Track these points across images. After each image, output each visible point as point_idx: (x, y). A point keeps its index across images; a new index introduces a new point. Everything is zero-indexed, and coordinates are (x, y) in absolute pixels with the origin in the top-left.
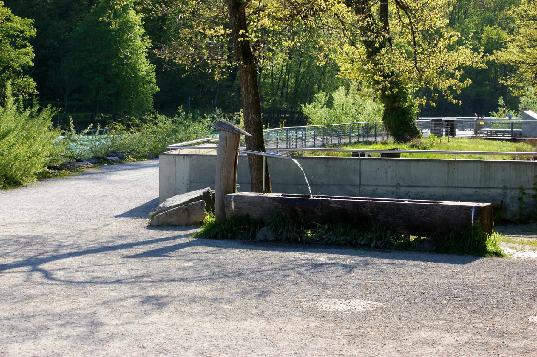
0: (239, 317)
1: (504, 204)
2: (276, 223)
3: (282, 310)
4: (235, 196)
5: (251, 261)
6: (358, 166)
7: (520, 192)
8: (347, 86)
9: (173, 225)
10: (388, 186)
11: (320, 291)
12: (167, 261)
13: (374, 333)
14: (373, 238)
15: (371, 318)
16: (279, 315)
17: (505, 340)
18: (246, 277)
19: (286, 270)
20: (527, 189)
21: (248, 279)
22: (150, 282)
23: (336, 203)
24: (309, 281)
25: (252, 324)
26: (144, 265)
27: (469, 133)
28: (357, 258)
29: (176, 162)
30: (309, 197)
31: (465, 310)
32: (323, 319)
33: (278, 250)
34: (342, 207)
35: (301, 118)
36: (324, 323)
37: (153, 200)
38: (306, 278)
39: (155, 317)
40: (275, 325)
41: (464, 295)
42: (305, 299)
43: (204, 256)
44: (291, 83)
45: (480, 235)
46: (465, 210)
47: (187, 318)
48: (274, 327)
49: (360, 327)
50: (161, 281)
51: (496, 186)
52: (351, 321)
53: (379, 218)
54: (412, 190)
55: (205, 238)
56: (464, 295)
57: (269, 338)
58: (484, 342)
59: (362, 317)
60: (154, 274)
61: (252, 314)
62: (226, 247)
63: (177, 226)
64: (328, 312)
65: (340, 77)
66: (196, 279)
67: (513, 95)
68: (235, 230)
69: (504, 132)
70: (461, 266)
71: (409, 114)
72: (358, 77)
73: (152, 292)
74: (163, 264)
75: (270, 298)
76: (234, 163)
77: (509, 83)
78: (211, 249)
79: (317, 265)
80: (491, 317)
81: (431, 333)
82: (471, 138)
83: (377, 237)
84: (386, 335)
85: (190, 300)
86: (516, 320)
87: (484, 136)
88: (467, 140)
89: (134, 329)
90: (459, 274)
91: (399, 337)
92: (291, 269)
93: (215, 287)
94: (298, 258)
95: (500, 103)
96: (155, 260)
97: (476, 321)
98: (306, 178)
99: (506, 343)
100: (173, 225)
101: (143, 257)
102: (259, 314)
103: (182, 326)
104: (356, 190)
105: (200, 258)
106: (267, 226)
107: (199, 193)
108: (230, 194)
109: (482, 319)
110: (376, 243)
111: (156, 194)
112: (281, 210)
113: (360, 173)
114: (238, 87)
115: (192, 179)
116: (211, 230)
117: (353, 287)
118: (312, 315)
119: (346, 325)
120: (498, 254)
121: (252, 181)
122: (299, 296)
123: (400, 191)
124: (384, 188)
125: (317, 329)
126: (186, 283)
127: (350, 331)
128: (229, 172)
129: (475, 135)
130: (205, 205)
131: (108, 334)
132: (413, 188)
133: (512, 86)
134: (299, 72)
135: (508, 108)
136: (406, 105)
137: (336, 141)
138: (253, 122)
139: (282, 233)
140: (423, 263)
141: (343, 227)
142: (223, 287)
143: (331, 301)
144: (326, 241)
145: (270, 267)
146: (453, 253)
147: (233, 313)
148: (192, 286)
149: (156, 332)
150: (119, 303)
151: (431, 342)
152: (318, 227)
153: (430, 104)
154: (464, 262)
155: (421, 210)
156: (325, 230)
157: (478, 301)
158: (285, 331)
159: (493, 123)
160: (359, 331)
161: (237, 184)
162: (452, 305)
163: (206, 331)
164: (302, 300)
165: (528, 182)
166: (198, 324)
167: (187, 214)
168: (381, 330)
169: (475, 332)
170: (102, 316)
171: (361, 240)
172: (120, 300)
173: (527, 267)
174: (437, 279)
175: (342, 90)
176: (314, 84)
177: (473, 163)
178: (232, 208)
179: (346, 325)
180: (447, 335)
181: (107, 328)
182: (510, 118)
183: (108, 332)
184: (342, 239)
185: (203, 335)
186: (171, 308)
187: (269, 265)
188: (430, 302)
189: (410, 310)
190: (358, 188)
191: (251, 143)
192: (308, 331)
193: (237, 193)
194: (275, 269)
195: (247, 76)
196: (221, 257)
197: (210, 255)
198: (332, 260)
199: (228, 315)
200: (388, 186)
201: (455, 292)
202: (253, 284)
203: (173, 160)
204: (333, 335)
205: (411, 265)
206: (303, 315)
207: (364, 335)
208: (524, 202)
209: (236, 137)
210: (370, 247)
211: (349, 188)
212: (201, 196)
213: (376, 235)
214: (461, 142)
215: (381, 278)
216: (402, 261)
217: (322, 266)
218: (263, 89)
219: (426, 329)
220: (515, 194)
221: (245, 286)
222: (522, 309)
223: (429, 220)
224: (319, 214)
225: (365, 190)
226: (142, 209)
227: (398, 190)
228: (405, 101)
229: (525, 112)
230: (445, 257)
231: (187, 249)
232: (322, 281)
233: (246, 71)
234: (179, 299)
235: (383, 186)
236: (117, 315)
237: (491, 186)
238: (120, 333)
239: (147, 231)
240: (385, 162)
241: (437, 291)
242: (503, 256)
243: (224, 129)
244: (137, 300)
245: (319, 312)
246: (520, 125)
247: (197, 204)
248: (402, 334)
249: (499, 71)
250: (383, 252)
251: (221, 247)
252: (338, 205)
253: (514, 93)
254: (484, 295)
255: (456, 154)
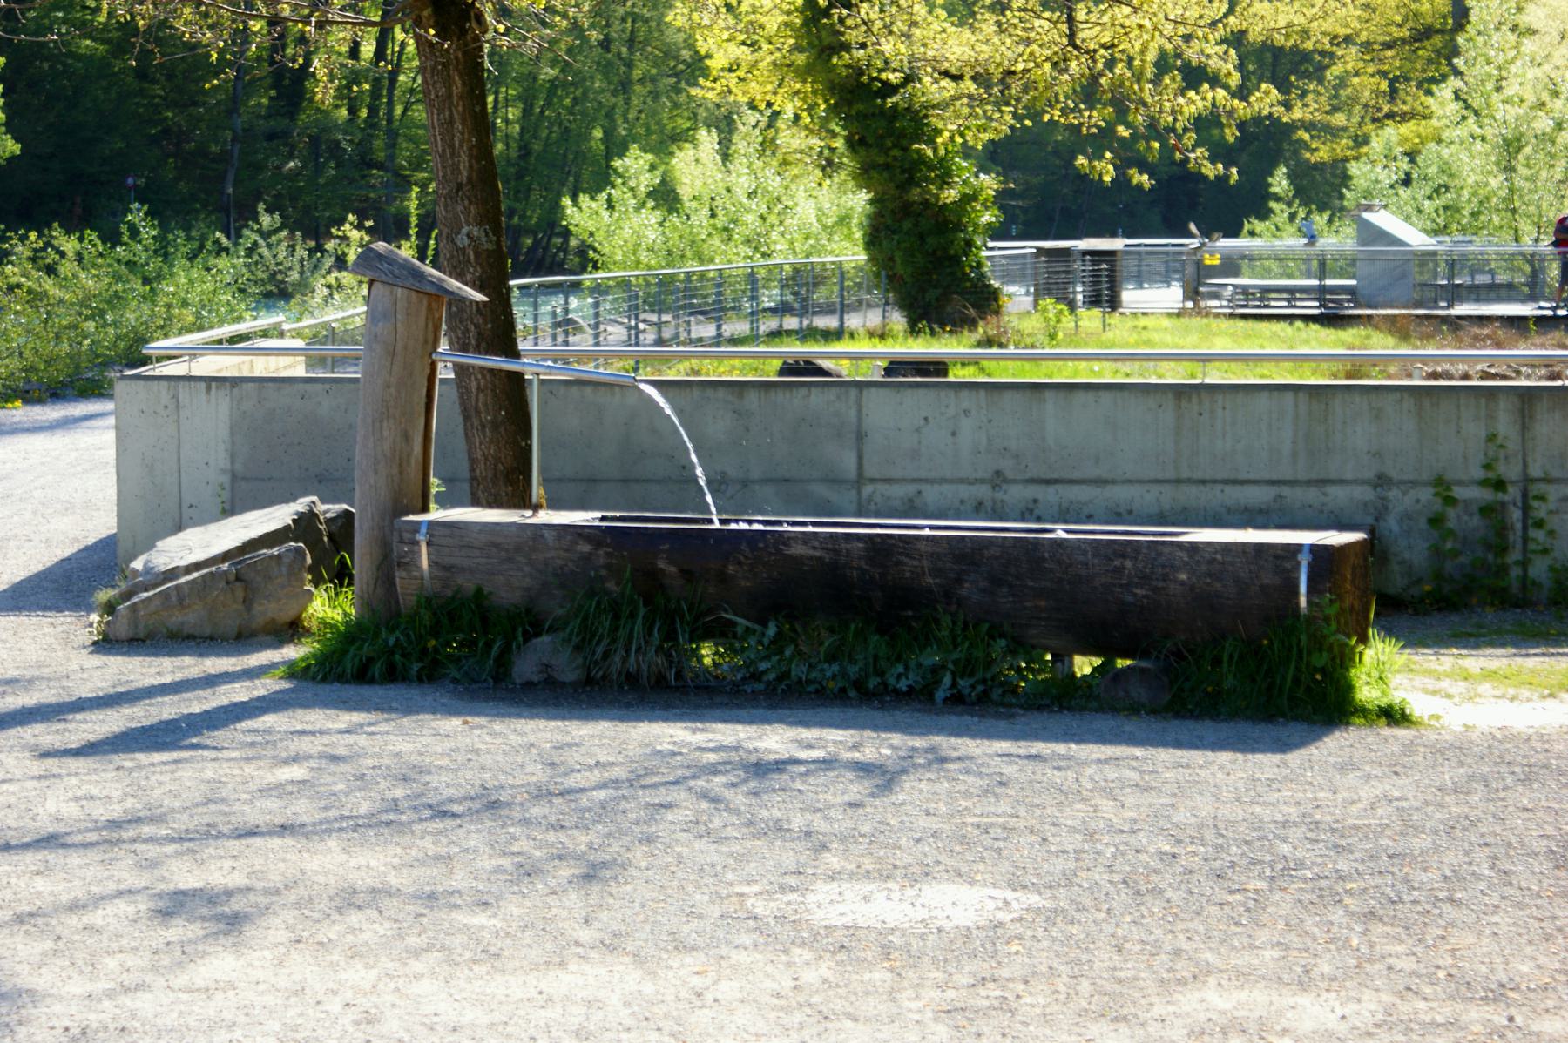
0: (535, 954)
1: (1379, 539)
2: (585, 619)
3: (686, 929)
4: (431, 524)
5: (519, 759)
6: (853, 413)
7: (1435, 495)
8: (725, 124)
9: (191, 637)
10: (962, 481)
11: (802, 859)
12: (210, 765)
13: (1042, 1001)
14: (943, 667)
15: (1014, 949)
16: (683, 947)
17: (1513, 1011)
18: (517, 814)
19: (655, 786)
20: (1460, 483)
21: (526, 822)
22: (172, 840)
23: (805, 543)
24: (750, 823)
25: (591, 980)
26: (127, 781)
27: (1171, 295)
28: (896, 738)
29: (178, 407)
30: (710, 521)
31: (1341, 912)
32: (842, 956)
33: (603, 718)
34: (827, 557)
35: (546, 249)
36: (849, 968)
37: (87, 549)
38: (738, 812)
39: (221, 964)
40: (673, 981)
41: (1319, 860)
42: (756, 888)
43: (342, 745)
44: (507, 121)
45: (1330, 649)
46: (1277, 557)
47: (342, 963)
48: (673, 990)
49: (984, 979)
50: (208, 835)
51: (1349, 476)
52: (946, 961)
53: (964, 592)
54: (1050, 495)
55: (324, 680)
56: (1319, 860)
57: (665, 1024)
58: (1440, 1019)
59: (982, 945)
60: (173, 811)
61: (577, 944)
62: (408, 710)
63: (205, 639)
64: (853, 930)
65: (710, 95)
66: (337, 825)
67: (1313, 160)
68: (434, 647)
69: (1291, 291)
70: (1276, 758)
71: (959, 227)
72: (775, 93)
73: (185, 875)
74: (197, 775)
75: (629, 888)
76: (424, 400)
77: (1297, 114)
78: (356, 717)
79: (762, 769)
80: (1440, 932)
81: (1243, 995)
82: (1179, 315)
83: (955, 662)
84: (1084, 1004)
85: (338, 902)
86: (1530, 942)
87: (1222, 307)
88: (1166, 322)
89: (159, 1009)
90: (1279, 786)
91: (1133, 1010)
92: (674, 783)
93: (414, 852)
94: (686, 745)
95: (1275, 189)
96: (165, 763)
97: (1390, 949)
98: (694, 458)
99: (1519, 1020)
100: (191, 637)
101: (115, 751)
102: (607, 942)
103: (335, 993)
104: (848, 497)
105: (329, 750)
106: (552, 629)
107: (279, 516)
108: (412, 518)
109: (1410, 942)
110: (954, 684)
111: (102, 523)
112: (603, 572)
113: (860, 436)
114: (309, 136)
115: (238, 467)
116: (347, 652)
117: (918, 840)
118: (798, 941)
119: (932, 975)
120: (1393, 716)
121: (472, 470)
122: (730, 876)
123: (1005, 497)
124: (946, 488)
125: (831, 993)
126: (303, 841)
127: (951, 994)
128: (407, 437)
129: (1190, 304)
130: (309, 561)
131: (67, 1029)
132: (1051, 489)
133: (1309, 126)
134: (535, 79)
135: (1304, 203)
136: (951, 195)
137: (709, 330)
138: (477, 254)
139: (606, 655)
140: (1138, 752)
141: (832, 631)
142: (443, 851)
143: (853, 890)
144: (769, 683)
145: (595, 776)
146: (1235, 715)
147: (508, 941)
148: (330, 850)
149: (242, 1019)
150: (75, 918)
151: (1252, 1028)
152: (739, 630)
153: (1129, 181)
154: (1283, 747)
155: (1117, 563)
156: (766, 641)
157: (1378, 880)
158: (716, 1001)
159: (1251, 259)
160: (983, 992)
161: (434, 480)
162: (1288, 897)
163: (429, 1009)
164: (746, 889)
165: (1465, 457)
166: (392, 985)
167: (240, 593)
168: (1062, 989)
169: (1401, 988)
170: (27, 967)
171: (899, 676)
172: (74, 907)
173: (1508, 758)
174: (1206, 808)
175: (707, 140)
176: (590, 123)
177: (1265, 394)
178: (419, 568)
179: (932, 975)
180: (1304, 1000)
181: (58, 1008)
182: (1312, 239)
183: (67, 1023)
184: (829, 674)
185: (424, 1024)
186: (275, 930)
187: (590, 768)
188: (1208, 885)
189: (1143, 916)
190: (854, 492)
191: (467, 330)
192: (802, 1001)
193: (436, 514)
194: (616, 783)
195: (448, 83)
196: (404, 746)
197: (362, 740)
198: (810, 747)
199: (492, 950)
200: (962, 481)
201: (1284, 848)
202: (551, 836)
203: (165, 398)
204: (895, 1010)
205: (1099, 761)
206: (767, 944)
207: (1004, 1006)
208: (1451, 532)
209: (429, 305)
210: (931, 697)
211: (821, 490)
212: (287, 527)
213: (955, 656)
214: (1145, 328)
215: (1004, 807)
216: (1061, 748)
217: (782, 771)
218: (404, 145)
219: (1223, 982)
220: (1418, 501)
221: (522, 845)
222: (1539, 902)
223: (1144, 596)
224: (743, 583)
225: (877, 498)
226: (53, 581)
227: (999, 495)
228: (945, 180)
229: (1366, 215)
230: (1206, 728)
231: (269, 720)
232: (798, 822)
233: (444, 64)
234: (293, 898)
235: (943, 481)
236: (80, 963)
237: (1333, 476)
238: (112, 1027)
239: (98, 660)
240: (951, 393)
241: (1219, 848)
242: (1411, 722)
243: (384, 278)
244: (143, 907)
245: (822, 932)
246: (1349, 264)
247: (279, 557)
248: (1143, 1001)
249: (1253, 73)
250: (983, 716)
251: (391, 710)
252: (815, 548)
253: (1316, 150)
254: (1389, 857)
255: (1204, 361)
